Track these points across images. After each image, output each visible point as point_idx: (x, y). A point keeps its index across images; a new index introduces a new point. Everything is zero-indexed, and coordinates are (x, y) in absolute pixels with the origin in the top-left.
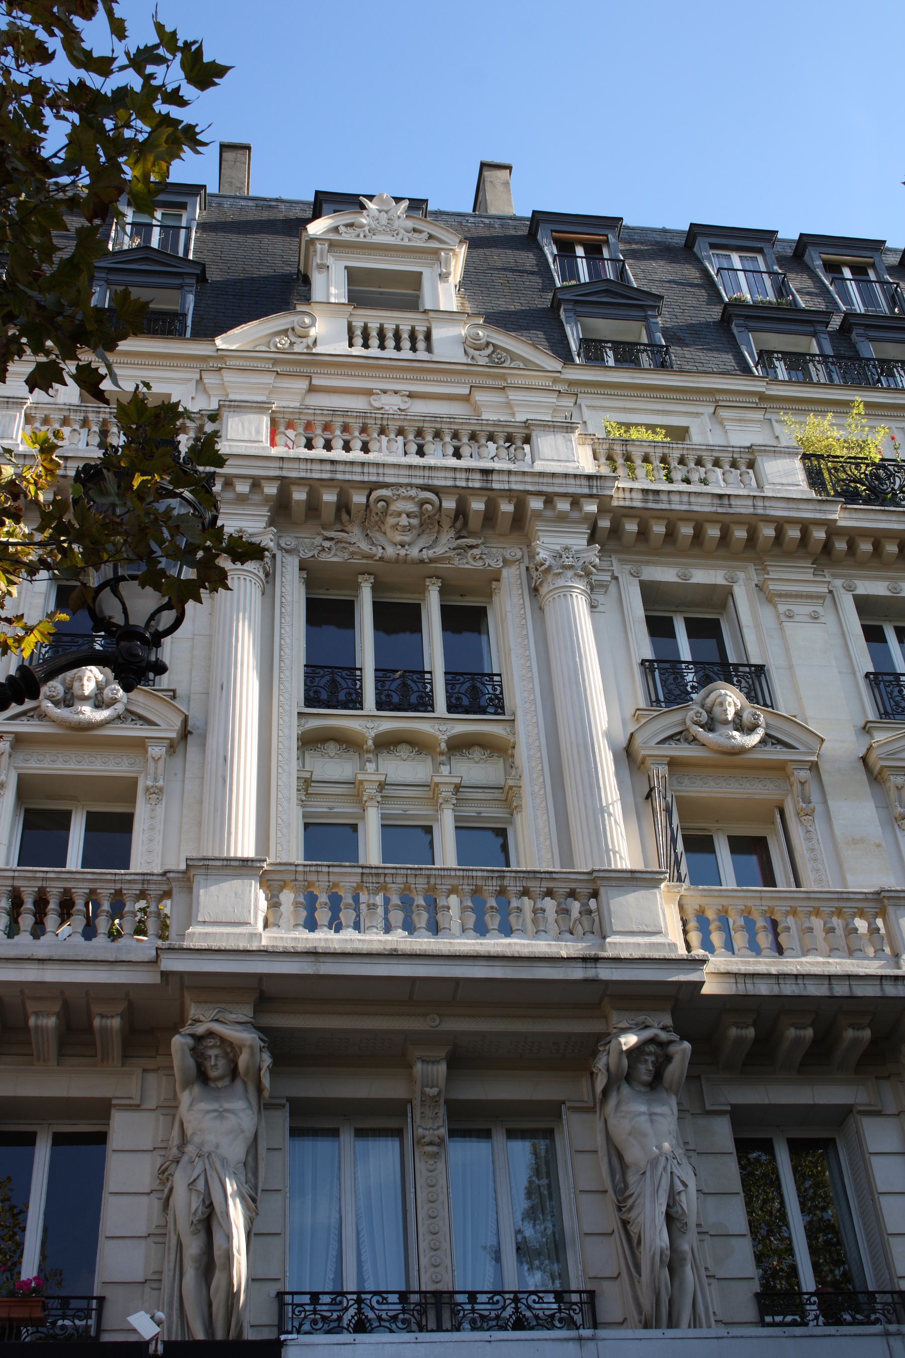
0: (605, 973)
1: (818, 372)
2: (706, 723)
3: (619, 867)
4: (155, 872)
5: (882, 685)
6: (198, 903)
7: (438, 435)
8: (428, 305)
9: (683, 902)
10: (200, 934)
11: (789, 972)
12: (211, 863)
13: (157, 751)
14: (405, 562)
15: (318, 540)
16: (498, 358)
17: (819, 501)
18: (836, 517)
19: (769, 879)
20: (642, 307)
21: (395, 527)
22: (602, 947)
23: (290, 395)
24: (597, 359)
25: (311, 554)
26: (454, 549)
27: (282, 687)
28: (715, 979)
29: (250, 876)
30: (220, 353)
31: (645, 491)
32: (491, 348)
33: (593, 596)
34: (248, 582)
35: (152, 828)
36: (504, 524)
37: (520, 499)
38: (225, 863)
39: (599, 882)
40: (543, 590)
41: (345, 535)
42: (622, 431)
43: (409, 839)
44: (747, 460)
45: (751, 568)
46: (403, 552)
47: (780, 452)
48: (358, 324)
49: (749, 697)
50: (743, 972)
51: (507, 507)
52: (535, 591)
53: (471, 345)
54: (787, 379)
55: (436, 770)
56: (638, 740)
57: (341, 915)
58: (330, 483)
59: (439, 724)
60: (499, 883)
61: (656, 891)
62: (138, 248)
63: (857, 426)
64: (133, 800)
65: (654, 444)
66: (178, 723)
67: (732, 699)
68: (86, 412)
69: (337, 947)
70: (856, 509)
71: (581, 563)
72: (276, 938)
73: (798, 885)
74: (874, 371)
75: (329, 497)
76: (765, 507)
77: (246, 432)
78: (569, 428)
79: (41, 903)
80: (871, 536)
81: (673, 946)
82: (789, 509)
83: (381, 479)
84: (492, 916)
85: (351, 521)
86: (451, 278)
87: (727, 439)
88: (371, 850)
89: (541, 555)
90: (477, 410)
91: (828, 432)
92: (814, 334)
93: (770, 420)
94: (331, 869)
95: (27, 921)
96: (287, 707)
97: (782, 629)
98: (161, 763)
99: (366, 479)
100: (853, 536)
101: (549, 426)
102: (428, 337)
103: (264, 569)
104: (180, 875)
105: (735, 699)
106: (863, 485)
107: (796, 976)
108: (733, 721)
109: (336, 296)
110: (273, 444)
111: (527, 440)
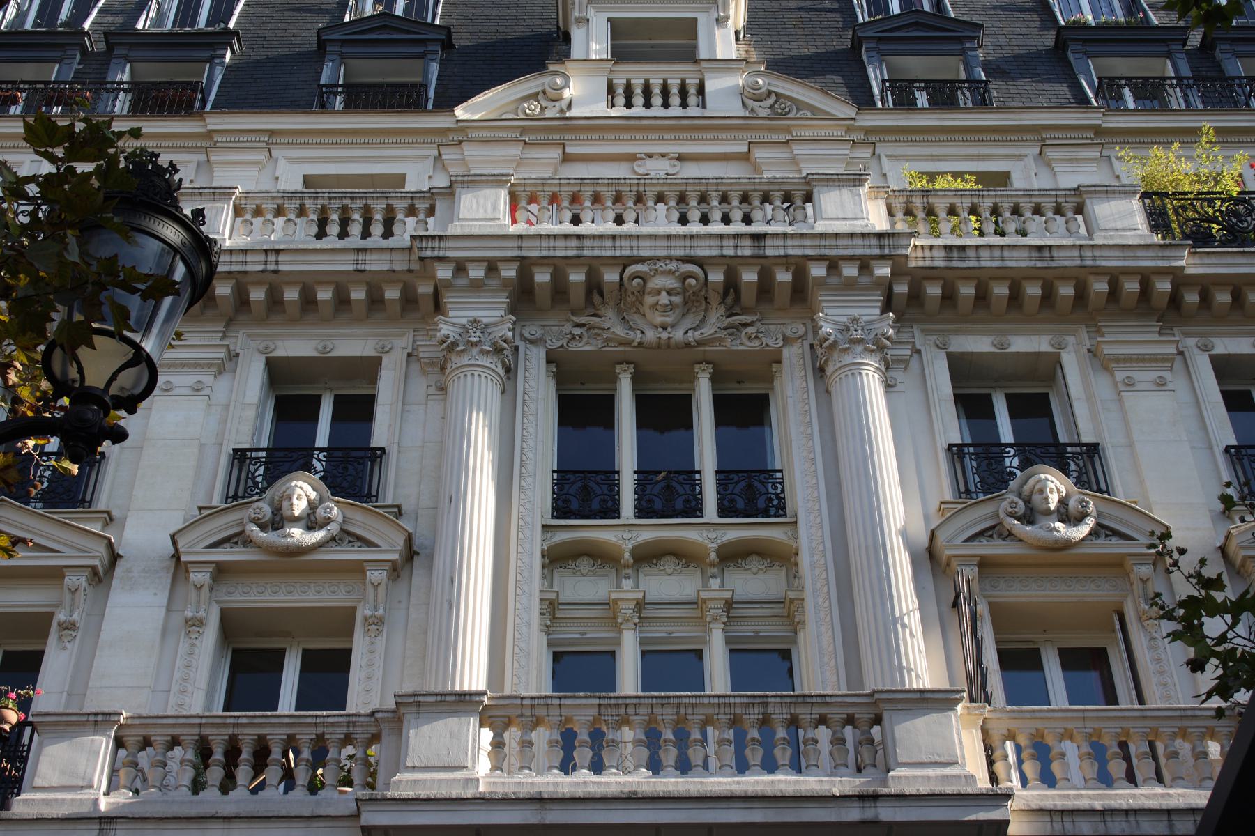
0: (887, 813)
1: (1176, 98)
2: (1024, 515)
3: (915, 686)
4: (362, 712)
5: (1246, 461)
6: (407, 746)
7: (597, 199)
8: (703, 53)
9: (988, 726)
10: (407, 781)
11: (1117, 806)
12: (422, 699)
13: (375, 575)
14: (668, 346)
15: (567, 328)
16: (781, 107)
17: (1161, 246)
18: (1183, 263)
19: (1111, 697)
20: (959, 39)
21: (655, 306)
22: (884, 783)
23: (541, 164)
24: (952, 104)
25: (559, 344)
26: (725, 329)
27: (523, 496)
28: (1024, 818)
29: (469, 713)
30: (460, 124)
31: (948, 248)
32: (773, 98)
33: (889, 374)
34: (476, 377)
35: (370, 665)
36: (782, 296)
37: (799, 266)
38: (439, 698)
39: (882, 705)
40: (829, 369)
41: (598, 319)
42: (924, 181)
43: (672, 667)
44: (1075, 204)
45: (1083, 332)
46: (664, 335)
47: (1114, 192)
48: (620, 81)
49: (1079, 482)
50: (1059, 808)
51: (784, 276)
52: (820, 372)
53: (749, 95)
54: (1184, 107)
55: (705, 585)
56: (941, 538)
57: (575, 754)
58: (576, 261)
59: (709, 530)
60: (762, 710)
61: (952, 714)
62: (381, 14)
63: (1208, 157)
64: (350, 634)
65: (961, 193)
66: (400, 541)
67: (1055, 486)
68: (302, 198)
69: (566, 791)
70: (1208, 253)
71: (872, 336)
72: (496, 783)
73: (1141, 701)
74: (1240, 91)
75: (577, 277)
76: (1094, 258)
77: (481, 210)
78: (857, 181)
79: (232, 753)
80: (1228, 284)
81: (971, 779)
82: (1124, 258)
83: (635, 253)
84: (753, 750)
85: (603, 303)
86: (730, 23)
87: (1056, 182)
88: (629, 679)
89: (443, 332)
90: (756, 168)
91: (1177, 168)
92: (1168, 55)
93: (1109, 157)
94: (563, 701)
95: (215, 774)
96: (528, 520)
97: (1120, 401)
98: (382, 589)
99: (618, 253)
100: (1206, 286)
101: (834, 180)
102: (701, 90)
103: (503, 363)
104: (390, 715)
105: (1058, 484)
106: (1218, 224)
107: (1126, 812)
108: (1058, 510)
109: (597, 52)
110: (514, 221)
111: (808, 198)
